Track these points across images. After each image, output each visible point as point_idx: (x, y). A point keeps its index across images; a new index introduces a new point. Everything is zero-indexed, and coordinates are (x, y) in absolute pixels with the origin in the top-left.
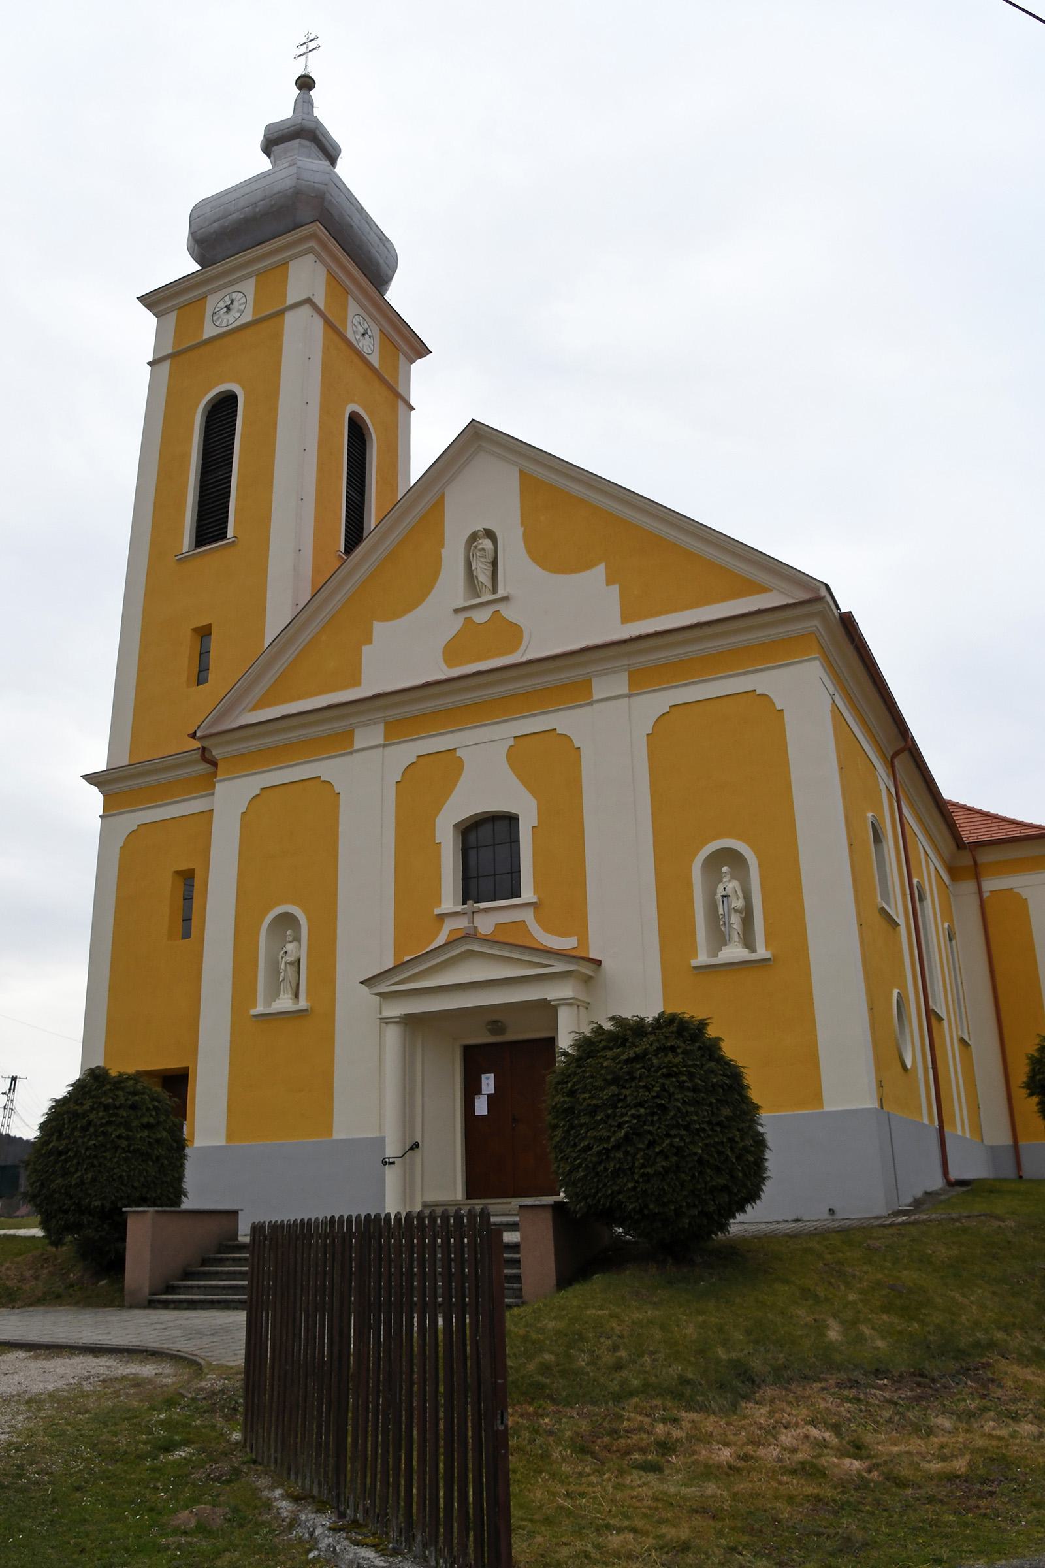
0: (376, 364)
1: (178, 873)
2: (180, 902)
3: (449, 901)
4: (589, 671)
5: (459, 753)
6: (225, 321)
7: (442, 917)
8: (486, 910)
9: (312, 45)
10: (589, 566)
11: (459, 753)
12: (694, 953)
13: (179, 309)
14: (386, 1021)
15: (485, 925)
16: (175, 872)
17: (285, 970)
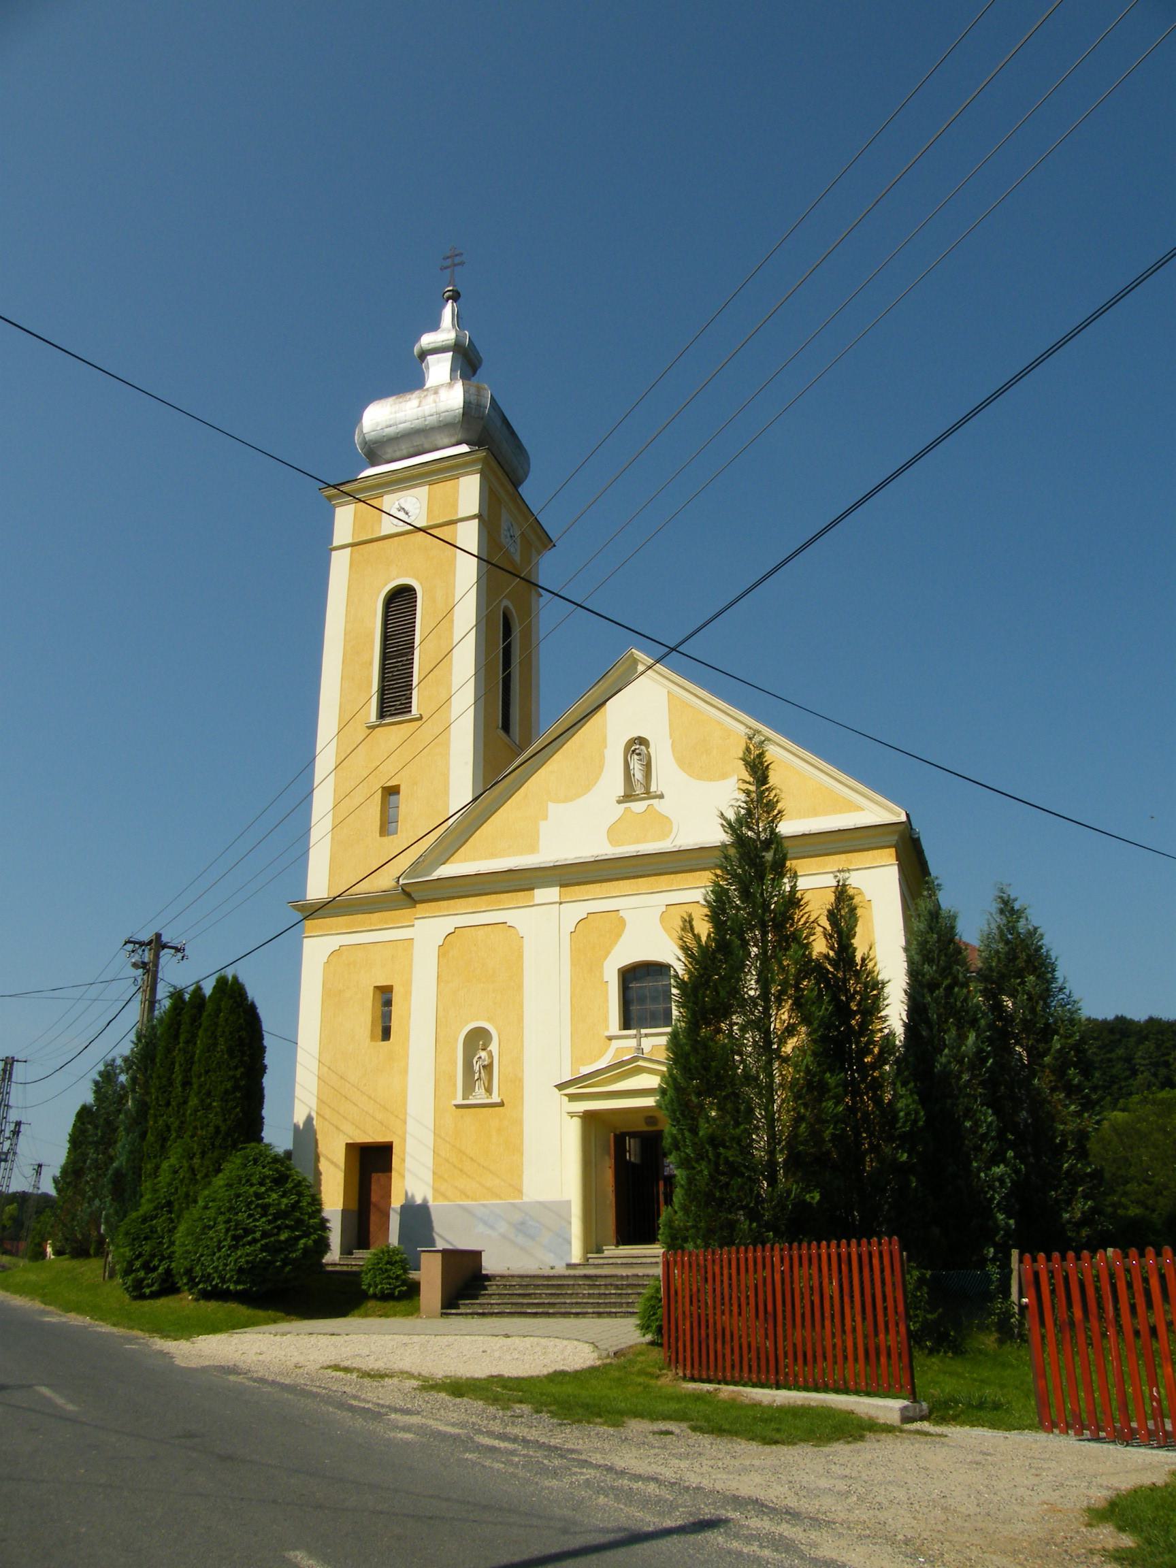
1: (378, 988)
2: (379, 1005)
5: (621, 913)
7: (610, 1038)
9: (457, 260)
11: (621, 913)
12: (455, 1098)
14: (572, 1115)
16: (375, 987)
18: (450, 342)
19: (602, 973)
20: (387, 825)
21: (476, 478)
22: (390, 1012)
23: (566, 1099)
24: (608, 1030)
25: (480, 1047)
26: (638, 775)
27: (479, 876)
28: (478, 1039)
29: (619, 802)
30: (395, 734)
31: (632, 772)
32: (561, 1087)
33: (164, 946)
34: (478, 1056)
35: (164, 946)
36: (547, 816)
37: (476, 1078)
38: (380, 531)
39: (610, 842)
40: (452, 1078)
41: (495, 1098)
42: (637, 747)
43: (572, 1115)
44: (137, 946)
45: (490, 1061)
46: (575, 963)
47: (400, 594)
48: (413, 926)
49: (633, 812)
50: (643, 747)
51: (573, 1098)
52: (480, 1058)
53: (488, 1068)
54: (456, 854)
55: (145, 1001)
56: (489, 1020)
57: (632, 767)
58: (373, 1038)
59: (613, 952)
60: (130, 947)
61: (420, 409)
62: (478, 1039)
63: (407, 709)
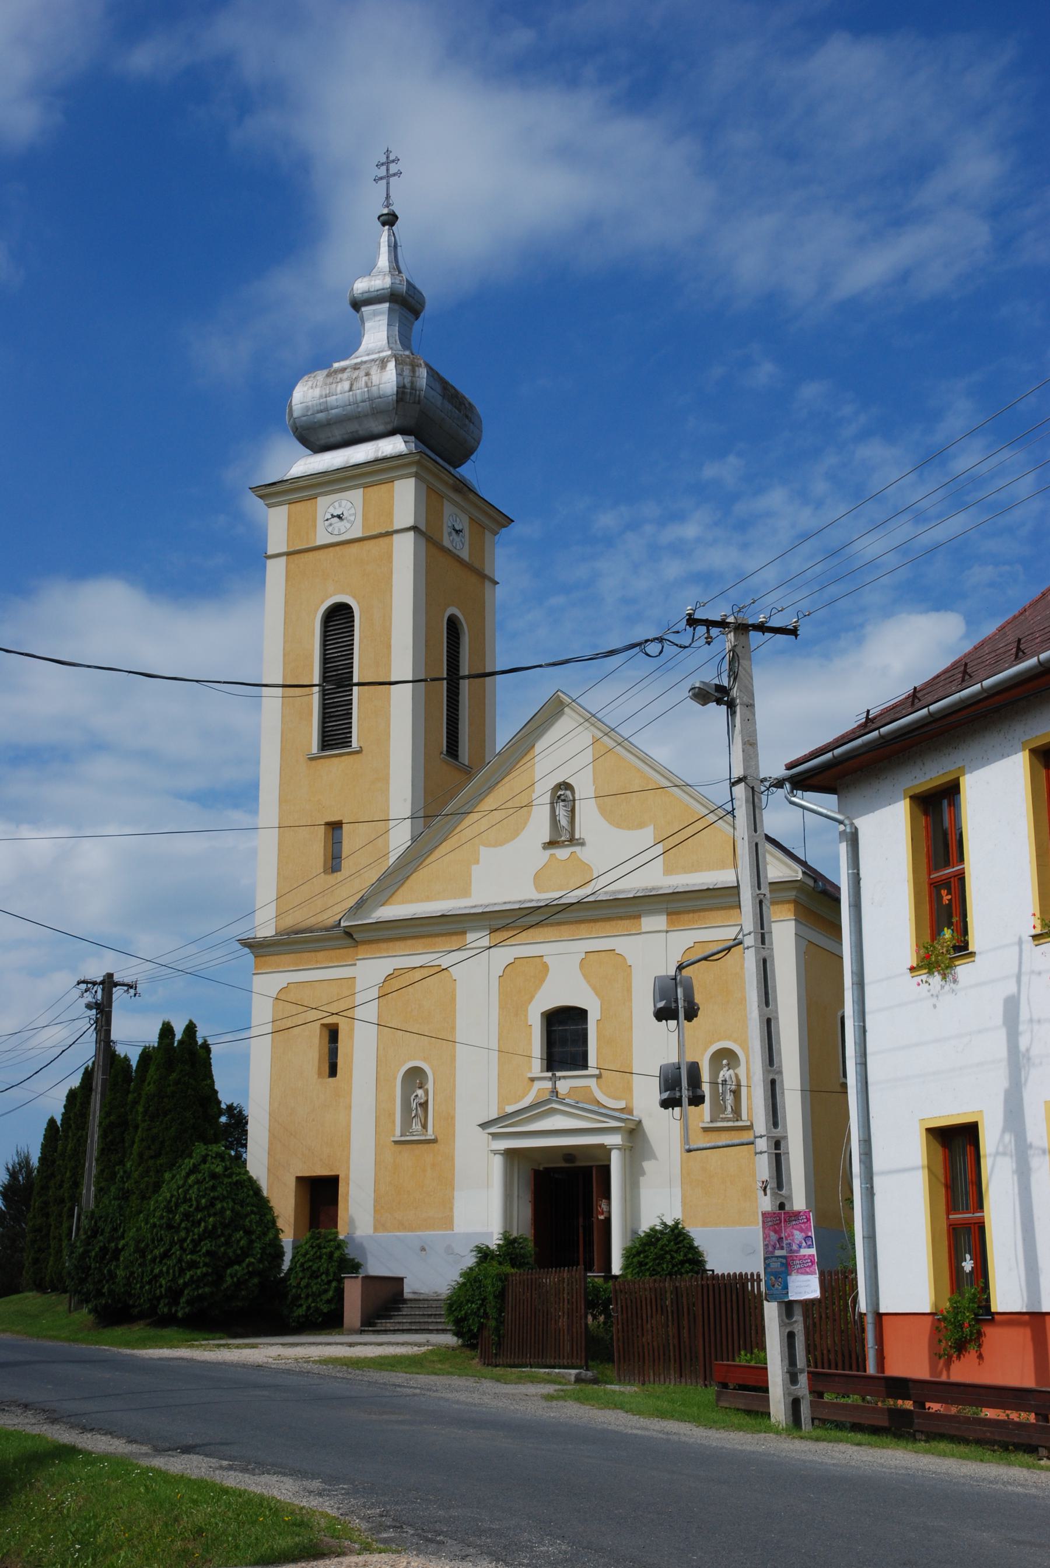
0: (467, 558)
2: (326, 1039)
3: (536, 1066)
4: (640, 909)
5: (545, 959)
6: (337, 529)
7: (532, 1080)
8: (564, 1077)
10: (641, 825)
11: (545, 959)
13: (289, 504)
14: (495, 1152)
15: (563, 1087)
17: (417, 1108)
18: (386, 291)
19: (526, 1016)
20: (334, 862)
21: (411, 483)
22: (337, 1048)
23: (490, 1137)
24: (531, 1072)
25: (417, 1085)
26: (564, 822)
27: (414, 920)
28: (415, 1077)
29: (544, 848)
30: (337, 766)
31: (558, 818)
32: (484, 1126)
33: (116, 985)
34: (415, 1094)
35: (116, 985)
36: (479, 860)
37: (413, 1115)
38: (315, 540)
39: (536, 888)
40: (391, 1115)
41: (430, 1134)
42: (562, 793)
43: (495, 1152)
44: (89, 985)
45: (425, 1098)
46: (502, 1007)
47: (340, 611)
48: (355, 965)
49: (557, 859)
50: (568, 793)
51: (494, 1136)
52: (417, 1096)
53: (424, 1105)
54: (394, 896)
55: (100, 1041)
56: (425, 1059)
57: (557, 814)
58: (320, 1074)
59: (537, 996)
60: (83, 986)
61: (351, 393)
62: (415, 1077)
63: (346, 742)
